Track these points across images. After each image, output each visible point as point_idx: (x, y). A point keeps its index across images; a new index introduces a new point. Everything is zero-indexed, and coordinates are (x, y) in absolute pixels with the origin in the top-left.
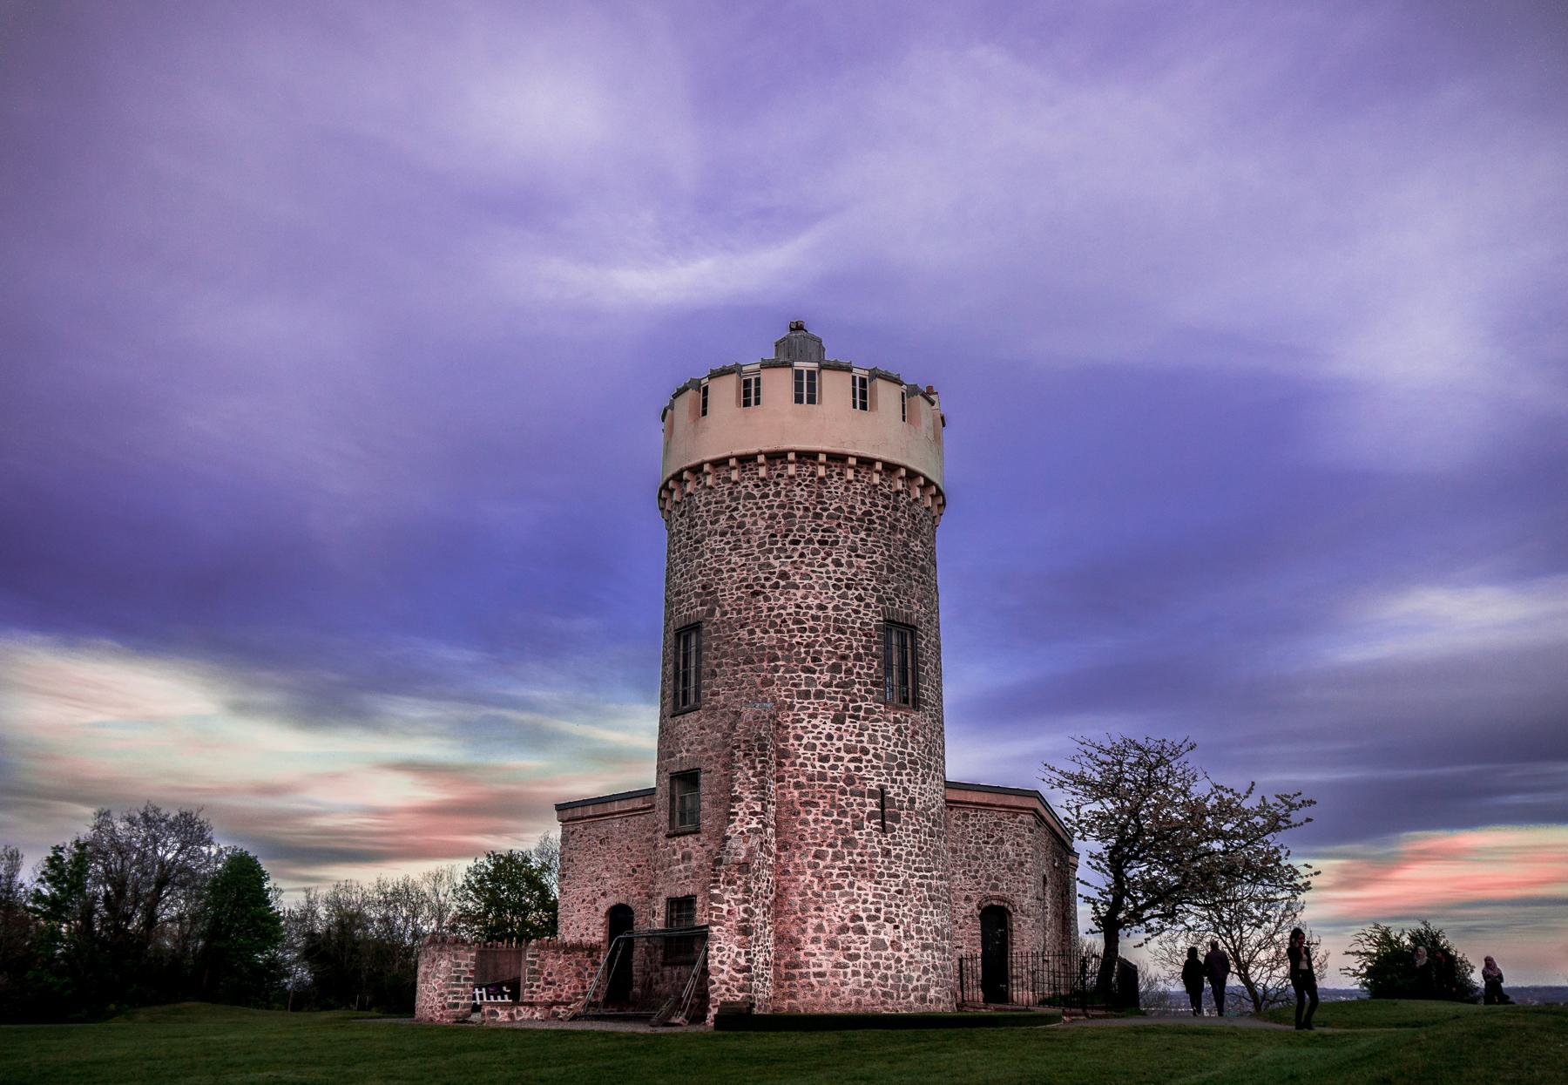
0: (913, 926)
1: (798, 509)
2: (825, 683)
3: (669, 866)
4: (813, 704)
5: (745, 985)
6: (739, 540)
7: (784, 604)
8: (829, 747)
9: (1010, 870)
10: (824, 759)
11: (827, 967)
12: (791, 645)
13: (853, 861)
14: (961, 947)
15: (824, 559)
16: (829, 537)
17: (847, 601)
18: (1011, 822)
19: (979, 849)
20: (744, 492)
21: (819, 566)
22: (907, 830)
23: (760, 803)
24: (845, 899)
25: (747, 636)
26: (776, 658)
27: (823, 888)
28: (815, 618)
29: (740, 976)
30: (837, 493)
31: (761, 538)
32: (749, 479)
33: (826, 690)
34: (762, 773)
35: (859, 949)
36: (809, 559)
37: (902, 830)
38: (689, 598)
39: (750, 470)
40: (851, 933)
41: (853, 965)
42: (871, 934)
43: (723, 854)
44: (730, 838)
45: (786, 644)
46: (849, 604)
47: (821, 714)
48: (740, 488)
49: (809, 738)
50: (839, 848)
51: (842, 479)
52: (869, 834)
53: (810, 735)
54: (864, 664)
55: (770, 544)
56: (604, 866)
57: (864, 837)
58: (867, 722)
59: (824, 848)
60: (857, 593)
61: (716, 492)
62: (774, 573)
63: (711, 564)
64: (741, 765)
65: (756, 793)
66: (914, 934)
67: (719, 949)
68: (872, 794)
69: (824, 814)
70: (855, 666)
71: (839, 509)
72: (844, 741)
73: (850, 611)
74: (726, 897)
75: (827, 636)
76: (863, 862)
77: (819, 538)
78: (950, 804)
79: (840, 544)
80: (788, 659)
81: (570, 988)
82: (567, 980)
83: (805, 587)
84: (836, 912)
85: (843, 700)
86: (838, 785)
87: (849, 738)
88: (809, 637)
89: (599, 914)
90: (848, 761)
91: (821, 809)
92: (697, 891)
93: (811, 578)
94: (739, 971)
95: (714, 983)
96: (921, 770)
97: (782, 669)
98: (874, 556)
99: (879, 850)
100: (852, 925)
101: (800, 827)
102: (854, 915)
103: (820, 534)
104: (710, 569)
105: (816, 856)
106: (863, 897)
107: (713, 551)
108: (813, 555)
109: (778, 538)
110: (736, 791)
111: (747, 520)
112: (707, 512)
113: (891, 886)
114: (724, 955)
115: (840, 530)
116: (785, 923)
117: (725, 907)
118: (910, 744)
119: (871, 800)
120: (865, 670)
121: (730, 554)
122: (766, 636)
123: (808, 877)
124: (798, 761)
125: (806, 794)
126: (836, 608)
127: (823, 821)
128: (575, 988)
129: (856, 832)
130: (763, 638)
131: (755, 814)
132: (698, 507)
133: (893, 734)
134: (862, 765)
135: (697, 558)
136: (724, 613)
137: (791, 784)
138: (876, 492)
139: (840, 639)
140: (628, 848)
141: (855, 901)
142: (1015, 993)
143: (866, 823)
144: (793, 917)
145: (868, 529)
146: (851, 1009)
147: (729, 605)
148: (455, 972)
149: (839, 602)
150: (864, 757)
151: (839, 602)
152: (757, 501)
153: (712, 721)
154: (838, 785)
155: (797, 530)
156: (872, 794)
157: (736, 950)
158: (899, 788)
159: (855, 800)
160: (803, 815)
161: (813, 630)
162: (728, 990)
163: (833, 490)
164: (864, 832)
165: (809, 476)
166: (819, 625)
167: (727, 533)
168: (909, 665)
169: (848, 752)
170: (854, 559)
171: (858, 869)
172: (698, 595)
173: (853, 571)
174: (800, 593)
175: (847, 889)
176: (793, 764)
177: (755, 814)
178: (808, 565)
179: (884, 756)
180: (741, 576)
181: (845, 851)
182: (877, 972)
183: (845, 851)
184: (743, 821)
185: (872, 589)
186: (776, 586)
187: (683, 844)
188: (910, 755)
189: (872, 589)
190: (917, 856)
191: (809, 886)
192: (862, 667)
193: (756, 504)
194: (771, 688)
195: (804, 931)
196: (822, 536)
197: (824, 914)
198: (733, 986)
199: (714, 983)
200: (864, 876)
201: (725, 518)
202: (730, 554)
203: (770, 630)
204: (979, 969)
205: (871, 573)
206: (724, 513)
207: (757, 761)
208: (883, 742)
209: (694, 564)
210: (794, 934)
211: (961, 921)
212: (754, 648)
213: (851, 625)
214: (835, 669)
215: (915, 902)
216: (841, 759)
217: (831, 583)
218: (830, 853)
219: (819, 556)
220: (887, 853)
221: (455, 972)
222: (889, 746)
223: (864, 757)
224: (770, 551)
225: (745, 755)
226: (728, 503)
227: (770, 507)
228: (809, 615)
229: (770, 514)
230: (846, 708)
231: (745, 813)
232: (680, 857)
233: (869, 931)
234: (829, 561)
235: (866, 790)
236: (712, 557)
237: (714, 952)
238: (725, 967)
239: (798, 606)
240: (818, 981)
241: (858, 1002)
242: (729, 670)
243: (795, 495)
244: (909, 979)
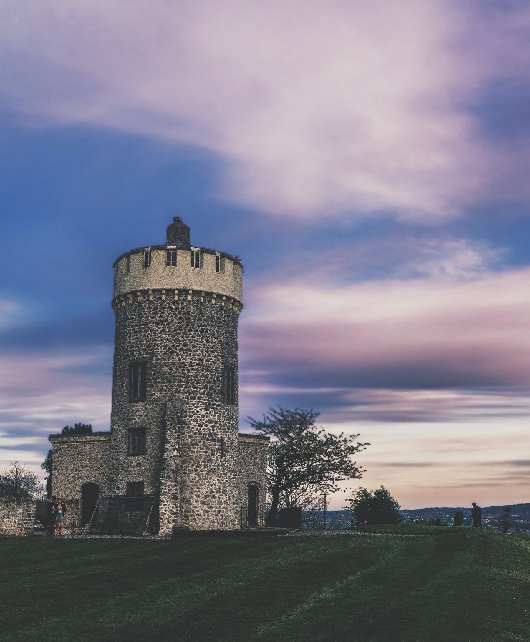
0: (231, 495)
1: (192, 316)
2: (201, 393)
3: (128, 468)
4: (197, 402)
5: (175, 520)
6: (165, 327)
7: (186, 358)
8: (203, 421)
9: (259, 470)
10: (201, 426)
11: (201, 512)
12: (188, 376)
13: (211, 469)
14: (241, 503)
15: (202, 339)
16: (204, 329)
17: (210, 358)
18: (260, 450)
19: (249, 462)
20: (167, 306)
21: (200, 342)
22: (230, 455)
23: (178, 444)
24: (208, 484)
25: (168, 371)
26: (182, 382)
27: (200, 480)
28: (198, 365)
29: (173, 516)
30: (207, 309)
31: (175, 327)
32: (170, 300)
33: (202, 396)
34: (179, 432)
35: (213, 505)
36: (196, 338)
37: (229, 455)
38: (139, 350)
39: (171, 296)
40: (210, 498)
41: (211, 511)
42: (217, 498)
43: (165, 466)
44: (166, 459)
45: (186, 376)
46: (212, 359)
47: (200, 406)
48: (166, 303)
49: (195, 416)
50: (206, 463)
51: (210, 303)
52: (217, 457)
53: (196, 415)
54: (217, 385)
55: (179, 331)
56: (80, 465)
57: (215, 459)
58: (217, 410)
59: (200, 463)
60: (215, 354)
61: (154, 304)
62: (181, 344)
63: (151, 336)
64: (169, 428)
65: (176, 440)
66: (231, 498)
67: (164, 505)
68: (218, 441)
69: (201, 449)
70: (213, 386)
71: (208, 317)
72: (209, 418)
73: (212, 362)
74: (168, 483)
75: (203, 373)
76: (215, 469)
77: (200, 329)
78: (240, 443)
79: (209, 332)
80: (187, 382)
81: (69, 520)
82: (68, 516)
83: (194, 351)
84: (204, 490)
85: (208, 401)
86: (206, 436)
87: (210, 417)
88: (196, 373)
89: (77, 487)
90: (210, 427)
91: (200, 446)
92: (145, 479)
93: (197, 347)
94: (173, 514)
95: (162, 519)
96: (234, 430)
97: (184, 386)
98: (221, 338)
99: (220, 464)
100: (210, 495)
101: (191, 454)
102: (211, 491)
103: (201, 327)
104: (151, 339)
105: (197, 466)
106: (215, 483)
107: (152, 330)
108: (198, 337)
109: (183, 328)
110: (167, 439)
111: (169, 318)
112: (149, 312)
113: (224, 479)
114: (167, 507)
115: (208, 326)
116: (185, 494)
117: (167, 488)
118: (231, 420)
119: (218, 443)
120: (217, 388)
121: (161, 333)
122: (177, 371)
123: (194, 475)
124: (191, 426)
125: (193, 440)
126: (206, 361)
127: (200, 452)
128: (71, 520)
129: (213, 456)
130: (176, 372)
131: (176, 449)
132: (145, 309)
133: (226, 415)
134: (215, 429)
135: (143, 332)
136: (158, 359)
137: (188, 436)
138: (222, 309)
139: (208, 374)
140: (95, 458)
141: (211, 485)
142: (259, 521)
143: (216, 453)
144: (188, 491)
145: (219, 326)
146: (210, 529)
147: (160, 356)
148: (28, 514)
149: (208, 358)
150: (216, 425)
151: (208, 358)
152: (173, 310)
153: (152, 407)
154: (206, 436)
155: (191, 325)
156: (218, 441)
157: (172, 505)
158: (227, 438)
159: (212, 443)
160: (192, 449)
161: (197, 370)
162: (168, 522)
163: (206, 308)
164: (215, 456)
165: (196, 301)
166: (200, 368)
167: (159, 323)
168: (230, 385)
169: (210, 423)
170: (214, 339)
171: (213, 472)
172: (143, 349)
173: (213, 344)
174: (192, 353)
175: (209, 480)
176: (188, 427)
177: (176, 449)
178: (195, 341)
179: (223, 425)
180: (166, 344)
181: (208, 464)
182: (219, 514)
183: (208, 464)
184: (171, 451)
185: (220, 353)
186: (182, 349)
187: (137, 459)
188: (231, 424)
189: (220, 353)
190: (233, 466)
191: (194, 479)
192: (216, 387)
193: (173, 311)
194: (179, 394)
195: (192, 497)
196: (202, 329)
197: (200, 490)
198: (170, 520)
199: (162, 519)
200: (215, 475)
201: (159, 316)
202: (161, 333)
203: (179, 369)
204: (247, 512)
205: (220, 345)
206: (157, 314)
207: (177, 426)
208: (223, 419)
209: (142, 335)
210: (188, 498)
211: (242, 492)
212: (172, 376)
213: (212, 368)
214: (205, 387)
215: (232, 485)
216: (207, 426)
217: (205, 349)
218: (203, 465)
219: (200, 338)
220: (223, 465)
221: (28, 514)
222: (224, 420)
223: (216, 425)
224: (179, 334)
225: (171, 424)
226: (159, 309)
227: (179, 314)
228: (196, 363)
229: (179, 317)
230: (209, 404)
231: (171, 448)
232: (135, 465)
233: (217, 497)
234: (204, 340)
235: (216, 439)
236: (151, 333)
237: (162, 506)
238: (167, 513)
239: (191, 359)
240: (198, 518)
241: (213, 526)
242: (160, 385)
243: (191, 309)
244: (230, 516)
